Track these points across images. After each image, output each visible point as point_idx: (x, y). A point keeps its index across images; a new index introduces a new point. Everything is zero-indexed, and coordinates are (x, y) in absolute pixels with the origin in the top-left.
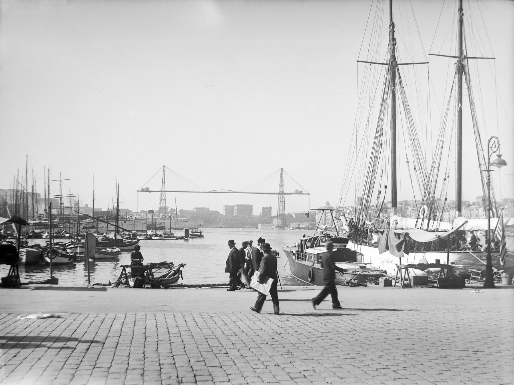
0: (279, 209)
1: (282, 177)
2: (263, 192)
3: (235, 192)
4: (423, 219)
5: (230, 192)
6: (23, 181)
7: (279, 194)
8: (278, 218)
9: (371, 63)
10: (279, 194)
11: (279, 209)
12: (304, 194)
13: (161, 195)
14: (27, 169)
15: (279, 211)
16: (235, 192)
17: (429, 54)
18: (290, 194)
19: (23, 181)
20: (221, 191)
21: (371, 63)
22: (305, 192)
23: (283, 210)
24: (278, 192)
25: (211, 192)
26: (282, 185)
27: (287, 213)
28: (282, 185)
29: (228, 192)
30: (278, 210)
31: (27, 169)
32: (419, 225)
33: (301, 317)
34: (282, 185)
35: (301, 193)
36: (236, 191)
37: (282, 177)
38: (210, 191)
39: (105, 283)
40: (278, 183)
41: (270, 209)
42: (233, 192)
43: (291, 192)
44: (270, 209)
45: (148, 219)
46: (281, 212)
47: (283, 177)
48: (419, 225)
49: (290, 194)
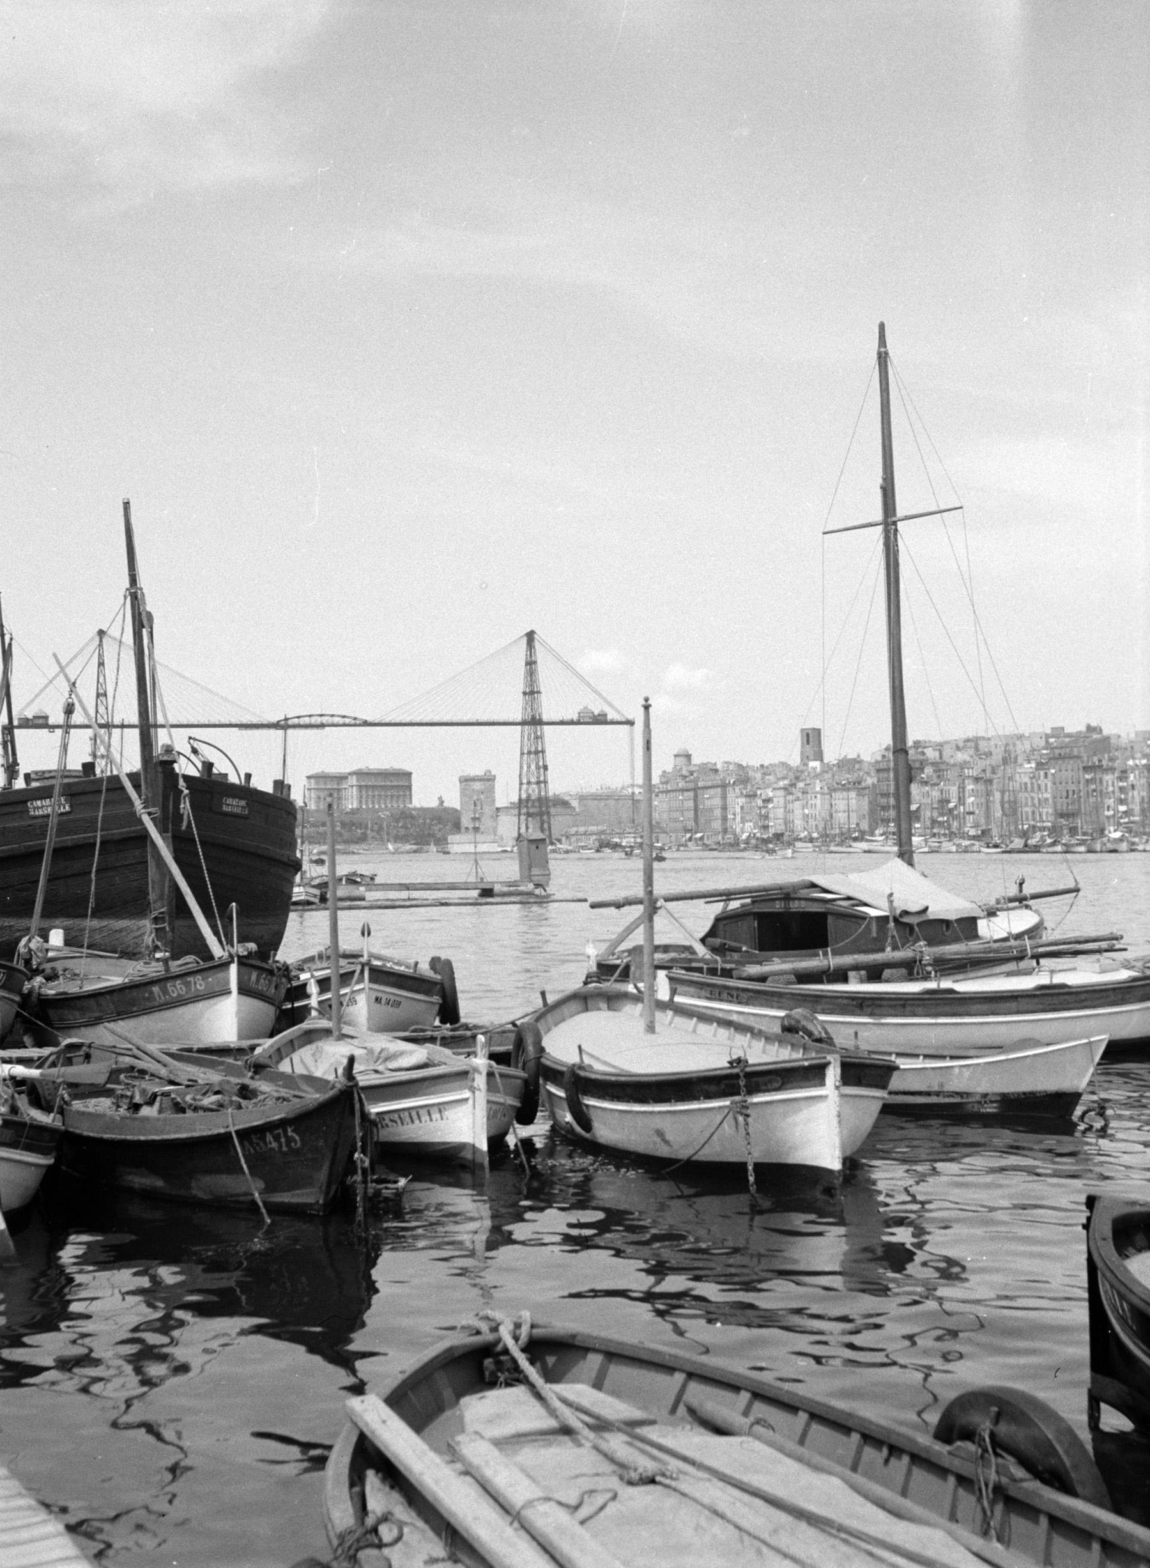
0: (525, 781)
1: (531, 664)
3: (366, 724)
5: (347, 721)
6: (540, 1236)
8: (524, 811)
10: (523, 723)
11: (525, 781)
12: (612, 723)
13: (95, 741)
15: (525, 787)
16: (366, 724)
17: (825, 533)
19: (540, 1236)
22: (618, 718)
23: (538, 783)
24: (519, 719)
26: (532, 693)
27: (551, 794)
28: (531, 693)
29: (341, 721)
30: (521, 784)
33: (833, 1547)
34: (531, 693)
35: (600, 720)
36: (370, 719)
37: (531, 664)
39: (711, 1204)
40: (520, 685)
41: (489, 779)
42: (358, 722)
43: (567, 717)
44: (489, 779)
46: (534, 791)
47: (535, 662)
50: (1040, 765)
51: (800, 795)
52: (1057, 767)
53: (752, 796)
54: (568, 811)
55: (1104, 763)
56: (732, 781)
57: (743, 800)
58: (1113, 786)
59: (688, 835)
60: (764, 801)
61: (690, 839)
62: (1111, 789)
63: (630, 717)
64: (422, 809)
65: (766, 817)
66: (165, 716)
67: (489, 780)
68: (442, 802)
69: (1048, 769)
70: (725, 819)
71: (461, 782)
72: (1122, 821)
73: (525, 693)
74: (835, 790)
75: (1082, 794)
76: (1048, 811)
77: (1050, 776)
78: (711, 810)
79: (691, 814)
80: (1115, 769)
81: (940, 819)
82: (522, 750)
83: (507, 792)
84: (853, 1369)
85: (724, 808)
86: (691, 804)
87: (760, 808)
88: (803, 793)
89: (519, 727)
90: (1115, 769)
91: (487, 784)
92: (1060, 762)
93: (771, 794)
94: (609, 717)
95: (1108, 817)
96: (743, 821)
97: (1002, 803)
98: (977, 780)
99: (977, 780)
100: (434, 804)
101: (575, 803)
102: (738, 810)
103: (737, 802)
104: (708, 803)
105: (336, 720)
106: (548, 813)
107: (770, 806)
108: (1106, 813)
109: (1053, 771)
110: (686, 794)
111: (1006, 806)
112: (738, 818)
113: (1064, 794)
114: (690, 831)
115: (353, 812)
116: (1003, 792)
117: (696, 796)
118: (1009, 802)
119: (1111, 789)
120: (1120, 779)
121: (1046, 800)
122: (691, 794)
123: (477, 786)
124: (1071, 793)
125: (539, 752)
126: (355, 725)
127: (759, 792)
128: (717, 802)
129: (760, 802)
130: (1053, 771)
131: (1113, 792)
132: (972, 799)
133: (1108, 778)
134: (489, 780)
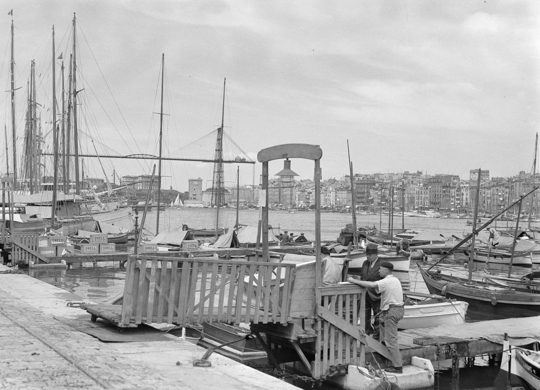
2: (195, 159)
4: (265, 210)
5: (152, 157)
7: (215, 161)
9: (162, 115)
10: (215, 161)
14: (12, 58)
18: (230, 162)
20: (140, 156)
21: (162, 115)
25: (126, 157)
28: (219, 150)
29: (141, 156)
31: (12, 58)
32: (21, 193)
34: (219, 150)
38: (125, 155)
41: (200, 180)
43: (231, 160)
44: (200, 180)
45: (372, 201)
48: (21, 193)
49: (230, 162)
50: (424, 185)
51: (324, 191)
52: (432, 186)
53: (304, 191)
54: (228, 193)
55: (451, 185)
56: (295, 186)
57: (300, 192)
58: (454, 193)
59: (276, 204)
60: (308, 193)
61: (277, 206)
62: (453, 195)
63: (254, 161)
64: (164, 190)
65: (309, 199)
66: (81, 152)
67: (200, 181)
68: (171, 188)
69: (428, 186)
70: (291, 199)
71: (189, 181)
72: (458, 207)
73: (216, 150)
74: (338, 190)
75: (441, 196)
76: (427, 202)
77: (428, 189)
78: (286, 196)
79: (278, 197)
80: (455, 187)
81: (382, 203)
82: (214, 170)
83: (207, 184)
84: (145, 343)
85: (292, 195)
86: (278, 193)
87: (306, 196)
88: (325, 191)
89: (213, 163)
90: (455, 187)
91: (199, 182)
92: (433, 184)
93: (311, 191)
94: (246, 160)
95: (452, 205)
96: (299, 200)
97: (408, 197)
98: (398, 189)
99: (398, 189)
100: (169, 188)
101: (230, 191)
102: (297, 196)
103: (297, 193)
104: (285, 193)
105: (148, 156)
106: (224, 194)
107: (311, 195)
108: (452, 203)
109: (430, 187)
110: (275, 189)
111: (410, 199)
112: (297, 199)
113: (434, 196)
114: (277, 203)
115: (140, 190)
116: (408, 194)
117: (280, 192)
118: (411, 197)
119: (453, 195)
120: (457, 191)
121: (427, 197)
122: (278, 189)
123: (196, 183)
124: (437, 195)
125: (221, 172)
126: (155, 159)
127: (306, 190)
128: (289, 192)
129: (306, 193)
130: (430, 187)
131: (454, 196)
132: (396, 196)
133: (453, 191)
134: (200, 181)
